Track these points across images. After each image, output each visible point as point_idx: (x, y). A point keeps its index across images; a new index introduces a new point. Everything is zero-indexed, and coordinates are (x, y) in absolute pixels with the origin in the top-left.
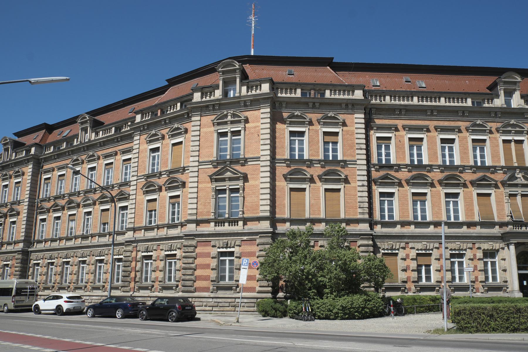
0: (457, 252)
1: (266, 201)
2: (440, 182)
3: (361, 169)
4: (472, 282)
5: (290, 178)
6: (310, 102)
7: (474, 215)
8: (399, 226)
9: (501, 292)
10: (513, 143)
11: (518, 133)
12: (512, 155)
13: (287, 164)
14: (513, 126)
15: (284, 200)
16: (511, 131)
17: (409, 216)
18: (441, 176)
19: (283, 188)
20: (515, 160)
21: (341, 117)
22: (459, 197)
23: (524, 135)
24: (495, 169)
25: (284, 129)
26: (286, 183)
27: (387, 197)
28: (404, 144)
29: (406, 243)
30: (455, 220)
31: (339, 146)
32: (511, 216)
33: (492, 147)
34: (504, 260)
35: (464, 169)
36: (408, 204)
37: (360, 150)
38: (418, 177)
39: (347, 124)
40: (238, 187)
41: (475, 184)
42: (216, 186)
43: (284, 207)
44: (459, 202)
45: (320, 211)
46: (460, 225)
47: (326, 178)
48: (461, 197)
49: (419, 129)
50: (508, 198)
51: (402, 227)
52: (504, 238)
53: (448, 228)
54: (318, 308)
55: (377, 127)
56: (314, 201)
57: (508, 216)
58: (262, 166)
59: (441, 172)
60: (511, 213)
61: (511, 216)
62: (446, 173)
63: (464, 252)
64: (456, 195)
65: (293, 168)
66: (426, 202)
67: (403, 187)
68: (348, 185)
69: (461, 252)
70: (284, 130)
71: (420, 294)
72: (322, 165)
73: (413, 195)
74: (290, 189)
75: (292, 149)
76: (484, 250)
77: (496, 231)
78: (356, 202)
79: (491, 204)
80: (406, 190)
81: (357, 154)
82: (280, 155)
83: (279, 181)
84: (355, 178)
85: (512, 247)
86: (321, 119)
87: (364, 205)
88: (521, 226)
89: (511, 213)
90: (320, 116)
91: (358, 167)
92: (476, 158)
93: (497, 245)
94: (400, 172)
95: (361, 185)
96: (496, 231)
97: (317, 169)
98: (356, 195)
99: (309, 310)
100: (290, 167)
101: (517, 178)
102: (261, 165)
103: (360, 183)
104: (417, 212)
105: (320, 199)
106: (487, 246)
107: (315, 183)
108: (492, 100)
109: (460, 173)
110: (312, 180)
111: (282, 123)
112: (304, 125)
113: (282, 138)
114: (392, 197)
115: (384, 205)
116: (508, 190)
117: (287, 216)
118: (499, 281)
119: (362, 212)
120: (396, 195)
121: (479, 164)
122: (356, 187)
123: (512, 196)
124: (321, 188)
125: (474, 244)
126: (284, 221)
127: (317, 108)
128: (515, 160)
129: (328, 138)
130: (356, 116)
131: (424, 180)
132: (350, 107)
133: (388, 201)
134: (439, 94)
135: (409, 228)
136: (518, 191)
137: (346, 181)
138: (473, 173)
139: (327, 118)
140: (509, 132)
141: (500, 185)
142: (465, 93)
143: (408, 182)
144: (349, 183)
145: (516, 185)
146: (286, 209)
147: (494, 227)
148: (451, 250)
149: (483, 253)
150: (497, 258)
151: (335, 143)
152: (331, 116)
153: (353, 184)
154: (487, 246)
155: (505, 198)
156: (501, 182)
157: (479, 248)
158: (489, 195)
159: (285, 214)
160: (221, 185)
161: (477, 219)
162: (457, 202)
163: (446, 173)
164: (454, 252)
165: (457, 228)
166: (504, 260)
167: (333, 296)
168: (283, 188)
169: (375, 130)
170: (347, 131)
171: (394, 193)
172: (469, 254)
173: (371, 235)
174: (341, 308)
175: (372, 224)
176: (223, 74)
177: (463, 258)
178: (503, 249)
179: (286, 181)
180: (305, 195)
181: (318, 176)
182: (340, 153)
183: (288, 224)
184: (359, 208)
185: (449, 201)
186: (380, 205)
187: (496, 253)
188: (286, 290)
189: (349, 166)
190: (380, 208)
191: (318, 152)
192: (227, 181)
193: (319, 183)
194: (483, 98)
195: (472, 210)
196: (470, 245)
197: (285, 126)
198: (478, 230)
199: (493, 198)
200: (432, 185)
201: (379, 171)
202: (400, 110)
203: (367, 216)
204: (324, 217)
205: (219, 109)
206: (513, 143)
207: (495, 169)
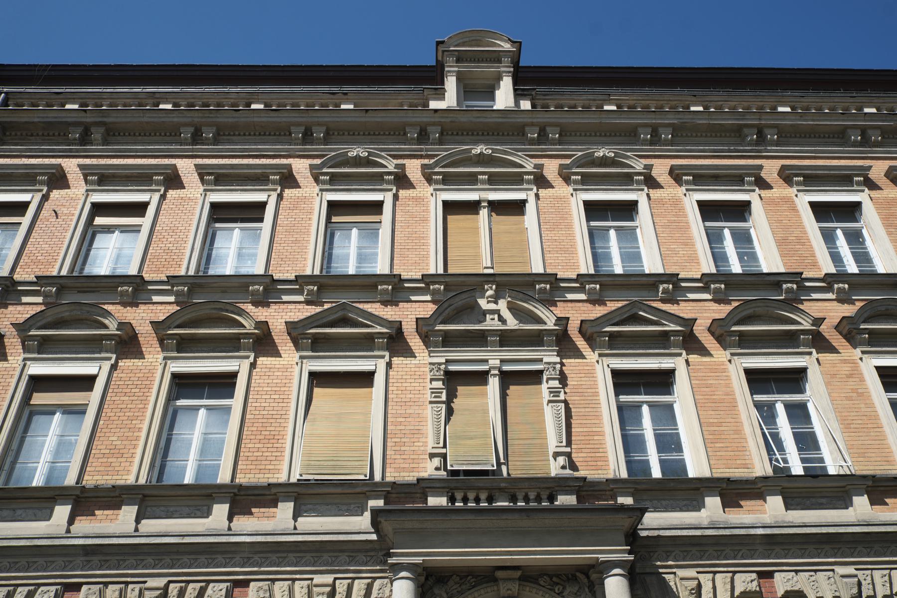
10: (484, 213)
11: (495, 181)
13: (590, 292)
14: (482, 160)
16: (474, 175)
22: (676, 388)
27: (780, 392)
33: (776, 225)
40: (484, 368)
41: (305, 336)
42: (447, 361)
47: (446, 332)
51: (725, 505)
55: (694, 176)
57: (432, 456)
101: (485, 313)
104: (643, 449)
115: (638, 420)
124: (599, 367)
125: (766, 575)
131: (90, 327)
133: (651, 405)
136: (486, 361)
140: (471, 180)
141: (415, 342)
145: (479, 339)
160: (466, 358)
162: (670, 407)
176: (458, 61)
183: (286, 509)
192: (493, 344)
200: (820, 343)
205: (326, 141)
206: (484, 213)
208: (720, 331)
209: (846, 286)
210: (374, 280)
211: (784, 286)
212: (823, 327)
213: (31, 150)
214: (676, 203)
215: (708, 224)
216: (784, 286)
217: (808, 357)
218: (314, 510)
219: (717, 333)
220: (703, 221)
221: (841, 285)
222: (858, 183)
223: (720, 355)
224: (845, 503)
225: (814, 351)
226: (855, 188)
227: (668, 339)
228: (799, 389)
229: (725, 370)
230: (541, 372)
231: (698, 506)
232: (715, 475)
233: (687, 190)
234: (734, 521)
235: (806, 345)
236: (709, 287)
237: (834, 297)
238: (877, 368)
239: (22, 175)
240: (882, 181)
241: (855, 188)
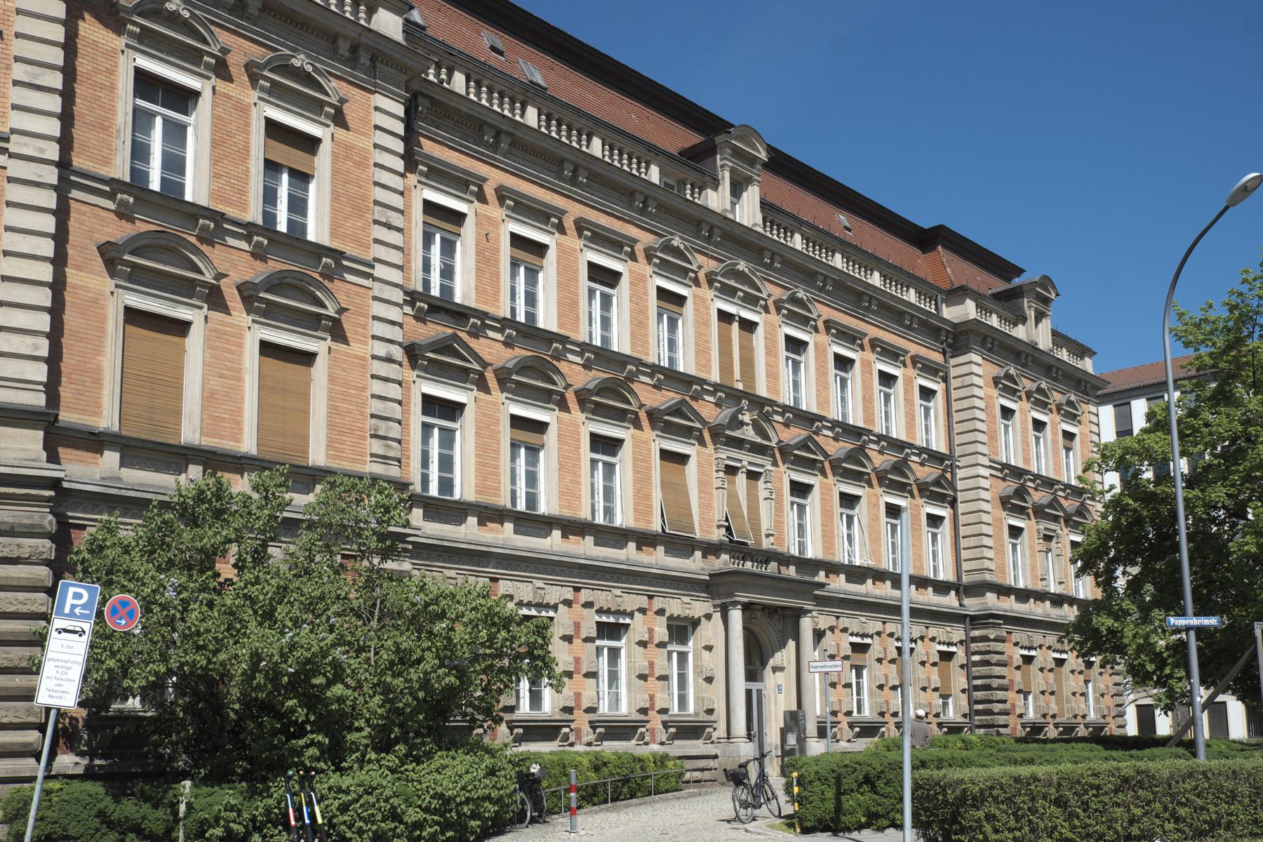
0: (612, 620)
1: (29, 340)
2: (248, 293)
3: (385, 296)
4: (965, 716)
6: (569, 161)
7: (651, 513)
8: (472, 520)
9: (700, 742)
10: (735, 325)
12: (732, 358)
15: (99, 351)
16: (736, 290)
17: (498, 489)
18: (255, 271)
19: (95, 301)
20: (737, 375)
21: (335, 88)
23: (758, 309)
24: (338, 264)
25: (114, 51)
28: (497, 250)
29: (492, 580)
30: (441, 491)
31: (316, 194)
32: (728, 529)
34: (709, 648)
36: (497, 451)
37: (385, 230)
38: (530, 367)
39: (349, 118)
40: (738, 465)
43: (98, 381)
45: (238, 424)
46: (544, 525)
47: (269, 302)
48: (626, 451)
49: (614, 243)
50: (721, 474)
52: (714, 587)
53: (516, 532)
54: (344, 808)
55: (431, 168)
56: (218, 381)
57: (719, 527)
58: (10, 180)
59: (584, 366)
60: (727, 520)
61: (728, 529)
62: (275, 265)
63: (551, 614)
64: (183, 98)
65: (142, 227)
66: (542, 454)
68: (342, 347)
69: (621, 621)
70: (112, 54)
71: (521, 749)
72: (122, 204)
73: (126, 321)
75: (140, 152)
76: (670, 618)
77: (695, 565)
78: (362, 413)
79: (685, 486)
80: (496, 404)
81: (377, 241)
82: (91, 158)
83: (79, 268)
84: (364, 327)
85: (736, 616)
86: (264, 66)
87: (389, 428)
88: (744, 559)
89: (727, 520)
90: (258, 53)
91: (378, 289)
92: (275, 204)
93: (698, 607)
94: (482, 340)
95: (382, 354)
96: (695, 565)
97: (235, 255)
98: (365, 388)
99: (312, 816)
100: (132, 220)
102: (10, 173)
103: (381, 349)
105: (240, 380)
106: (678, 606)
108: (701, 189)
109: (692, 398)
111: (107, 26)
112: (198, 64)
113: (103, 87)
114: (454, 420)
116: (726, 454)
117: (107, 419)
118: (691, 709)
119: (380, 452)
120: (469, 413)
121: (282, 227)
122: (363, 359)
123: (731, 471)
125: (577, 589)
126: (94, 441)
127: (248, 19)
128: (737, 375)
129: (284, 154)
130: (380, 100)
131: (544, 381)
132: (364, 60)
134: (590, 124)
135: (497, 531)
137: (337, 332)
138: (654, 386)
139: (668, 248)
142: (651, 148)
143: (503, 378)
144: (345, 341)
146: (106, 392)
147: (689, 554)
148: (600, 611)
149: (669, 627)
150: (691, 644)
151: (301, 178)
152: (302, 69)
153: (356, 348)
154: (678, 606)
155: (715, 475)
156: (650, 414)
157: (661, 612)
158: (308, 358)
159: (97, 413)
161: (656, 526)
162: (183, 128)
163: (275, 265)
164: (604, 619)
166: (709, 648)
167: (391, 760)
168: (95, 301)
169: (421, 173)
170: (348, 147)
171: (547, 424)
172: (638, 626)
173: (55, 484)
174: (435, 804)
175: (58, 438)
177: (619, 639)
178: (708, 617)
179: (112, 273)
181: (238, 288)
182: (319, 219)
183: (111, 458)
184: (374, 436)
186: (134, 130)
187: (690, 629)
188: (88, 744)
189: (349, 277)
191: (243, 192)
194: (682, 176)
195: (648, 497)
196: (568, 594)
197: (121, 42)
198: (658, 559)
199: (195, 342)
200: (215, 299)
201: (424, 321)
202: (498, 133)
203: (38, 400)
204: (116, 428)
208: (248, 293)
209: (131, 200)
210: (195, 211)
211: (201, 221)
212: (224, 283)
213: (452, 141)
214: (243, 110)
215: (140, 102)
216: (201, 221)
217: (197, 311)
218: (138, 464)
219: (246, 294)
220: (135, 96)
221: (125, 196)
222: (207, 66)
223: (239, 316)
224: (622, 546)
225: (206, 306)
226: (322, 119)
227: (194, 288)
228: (613, 453)
229: (241, 337)
230: (738, 468)
231: (546, 535)
232: (124, 433)
233: (127, 46)
234: (131, 480)
235: (200, 298)
236: (115, 195)
237: (247, 249)
238: (887, 503)
239: (540, 211)
240: (237, 69)
241: (322, 119)
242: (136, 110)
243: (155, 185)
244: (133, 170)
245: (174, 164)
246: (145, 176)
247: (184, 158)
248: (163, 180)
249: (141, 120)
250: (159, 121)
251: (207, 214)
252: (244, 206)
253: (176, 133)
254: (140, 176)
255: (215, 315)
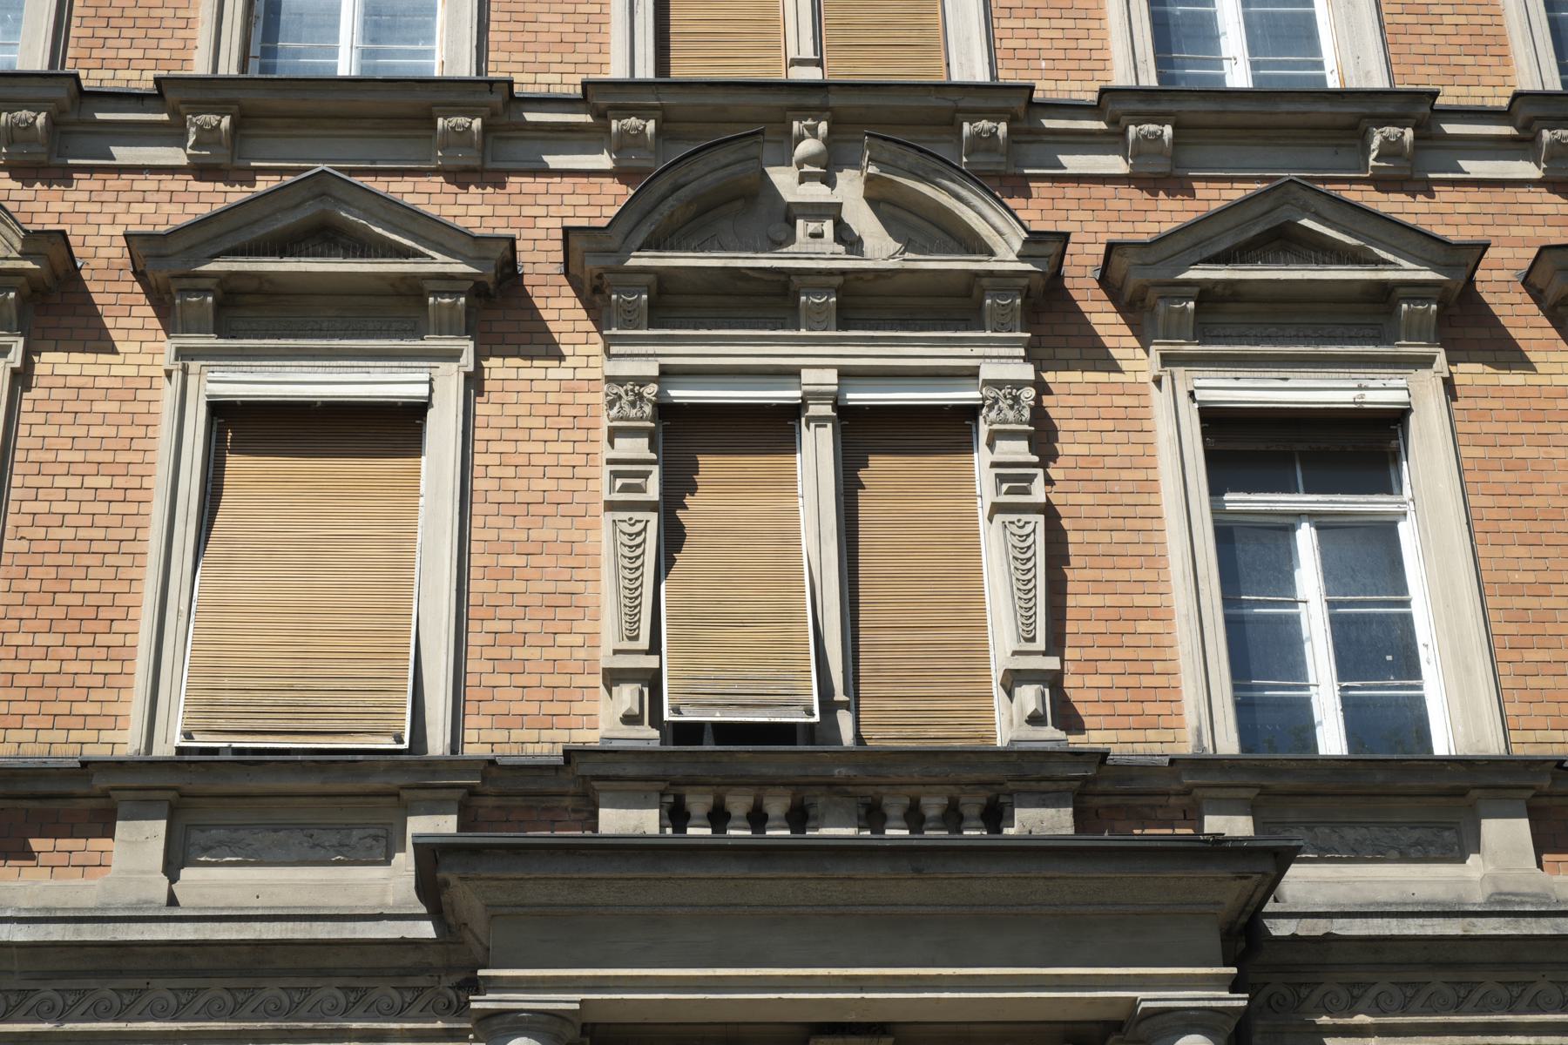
5: (663, 281)
26: (169, 346)
35: (1427, 135)
41: (194, 283)
44: (1406, 531)
47: (662, 275)
64: (1364, 448)
67: (1505, 352)
74: (221, 412)
75: (1258, 647)
101: (791, 214)
107: (537, 342)
110: (497, 309)
124: (1160, 401)
136: (793, 373)
145: (771, 301)
162: (1384, 532)
165: (1404, 858)
180: (412, 487)
185: (1282, 529)
186: (1230, 598)
190: (1235, 626)
193: (142, 345)
200: (1465, 326)
207: (1427, 135)
225: (1441, 355)
227: (1392, 311)
242: (1227, 533)
243: (1332, 740)
244: (1245, 708)
245: (1377, 647)
246: (1300, 718)
247: (1407, 620)
248: (1352, 709)
249: (1247, 555)
250: (1306, 538)
251: (1388, 108)
252: (1493, 44)
253: (1369, 554)
254: (1271, 720)
255: (1470, 374)
